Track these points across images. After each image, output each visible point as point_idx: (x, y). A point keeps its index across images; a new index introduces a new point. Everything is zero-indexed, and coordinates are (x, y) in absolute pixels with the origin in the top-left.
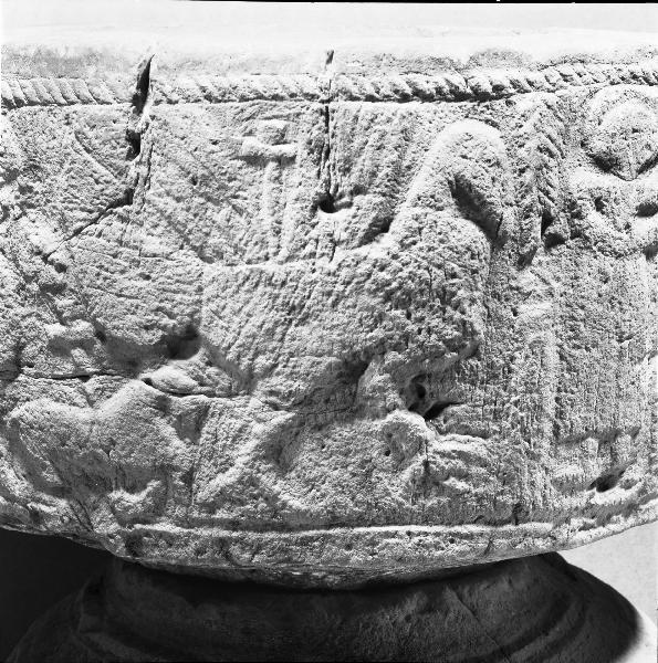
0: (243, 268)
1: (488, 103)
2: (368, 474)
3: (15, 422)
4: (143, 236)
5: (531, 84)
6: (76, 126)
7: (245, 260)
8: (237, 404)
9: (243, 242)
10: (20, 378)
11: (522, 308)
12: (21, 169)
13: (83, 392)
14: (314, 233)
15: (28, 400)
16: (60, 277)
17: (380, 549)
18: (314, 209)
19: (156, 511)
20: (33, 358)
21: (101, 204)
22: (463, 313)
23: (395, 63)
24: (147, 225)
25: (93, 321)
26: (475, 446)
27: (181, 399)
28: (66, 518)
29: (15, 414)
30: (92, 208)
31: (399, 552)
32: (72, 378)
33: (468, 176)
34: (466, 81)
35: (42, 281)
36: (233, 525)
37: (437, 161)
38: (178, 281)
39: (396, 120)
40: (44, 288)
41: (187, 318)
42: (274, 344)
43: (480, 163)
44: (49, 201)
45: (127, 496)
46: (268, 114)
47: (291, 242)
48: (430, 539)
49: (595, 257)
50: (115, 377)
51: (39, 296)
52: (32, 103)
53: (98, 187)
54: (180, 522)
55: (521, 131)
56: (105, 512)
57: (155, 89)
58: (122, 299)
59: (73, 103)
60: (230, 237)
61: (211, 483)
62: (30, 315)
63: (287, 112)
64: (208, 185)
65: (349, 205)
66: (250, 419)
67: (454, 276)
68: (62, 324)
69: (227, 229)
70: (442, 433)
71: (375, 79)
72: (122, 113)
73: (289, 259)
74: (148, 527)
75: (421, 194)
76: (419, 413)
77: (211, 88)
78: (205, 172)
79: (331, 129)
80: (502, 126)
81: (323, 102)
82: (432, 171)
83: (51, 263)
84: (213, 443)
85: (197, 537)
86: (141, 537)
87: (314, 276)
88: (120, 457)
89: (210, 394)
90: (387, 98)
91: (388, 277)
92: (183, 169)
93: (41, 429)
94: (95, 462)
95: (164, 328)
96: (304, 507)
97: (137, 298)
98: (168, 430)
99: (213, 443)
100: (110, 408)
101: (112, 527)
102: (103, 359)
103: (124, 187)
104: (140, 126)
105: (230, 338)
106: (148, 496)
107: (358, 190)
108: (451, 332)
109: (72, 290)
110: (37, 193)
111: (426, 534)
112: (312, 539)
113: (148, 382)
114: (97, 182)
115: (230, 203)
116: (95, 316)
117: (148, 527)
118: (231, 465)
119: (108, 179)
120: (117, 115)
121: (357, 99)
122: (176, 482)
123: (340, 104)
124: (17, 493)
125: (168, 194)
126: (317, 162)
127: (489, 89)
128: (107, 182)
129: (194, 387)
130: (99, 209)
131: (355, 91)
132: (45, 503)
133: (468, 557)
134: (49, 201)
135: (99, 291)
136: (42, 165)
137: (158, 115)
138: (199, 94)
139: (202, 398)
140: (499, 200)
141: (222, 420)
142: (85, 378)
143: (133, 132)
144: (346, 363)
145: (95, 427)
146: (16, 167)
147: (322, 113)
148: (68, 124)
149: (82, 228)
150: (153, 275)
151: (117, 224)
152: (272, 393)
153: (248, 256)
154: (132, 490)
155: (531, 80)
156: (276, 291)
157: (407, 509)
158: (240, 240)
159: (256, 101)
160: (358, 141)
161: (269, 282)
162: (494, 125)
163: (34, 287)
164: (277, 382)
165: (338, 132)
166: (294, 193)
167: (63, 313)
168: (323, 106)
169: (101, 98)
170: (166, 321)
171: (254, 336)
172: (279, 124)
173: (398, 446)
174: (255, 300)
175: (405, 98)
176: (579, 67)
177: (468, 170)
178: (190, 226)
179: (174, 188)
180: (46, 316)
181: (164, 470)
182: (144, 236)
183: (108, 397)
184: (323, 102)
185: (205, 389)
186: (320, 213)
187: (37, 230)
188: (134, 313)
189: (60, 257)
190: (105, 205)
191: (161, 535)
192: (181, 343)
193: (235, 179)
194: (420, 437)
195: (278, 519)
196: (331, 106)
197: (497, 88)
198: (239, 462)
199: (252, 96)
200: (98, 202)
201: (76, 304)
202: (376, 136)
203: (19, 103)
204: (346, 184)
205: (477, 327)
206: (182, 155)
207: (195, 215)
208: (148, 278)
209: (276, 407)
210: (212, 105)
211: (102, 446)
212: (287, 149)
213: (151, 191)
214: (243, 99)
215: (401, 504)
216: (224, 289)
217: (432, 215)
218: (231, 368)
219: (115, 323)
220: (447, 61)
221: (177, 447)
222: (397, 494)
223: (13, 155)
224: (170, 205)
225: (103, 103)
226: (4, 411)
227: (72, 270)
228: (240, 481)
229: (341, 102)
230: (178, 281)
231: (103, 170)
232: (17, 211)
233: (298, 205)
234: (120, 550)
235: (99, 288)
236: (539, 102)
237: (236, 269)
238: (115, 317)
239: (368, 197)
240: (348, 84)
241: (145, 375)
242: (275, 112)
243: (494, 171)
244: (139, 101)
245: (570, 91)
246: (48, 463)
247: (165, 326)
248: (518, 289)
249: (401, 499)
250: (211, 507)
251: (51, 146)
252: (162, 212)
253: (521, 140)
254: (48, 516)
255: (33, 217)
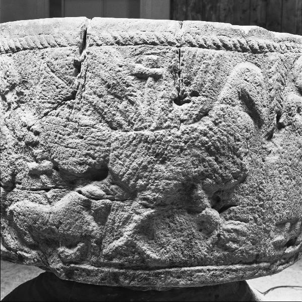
0: (132, 133)
1: (256, 55)
2: (190, 241)
3: (11, 212)
4: (81, 116)
5: (275, 48)
6: (47, 59)
7: (134, 128)
8: (126, 205)
9: (133, 119)
10: (14, 190)
11: (267, 158)
12: (18, 83)
13: (46, 197)
14: (170, 115)
15: (18, 200)
16: (36, 138)
17: (195, 278)
18: (171, 102)
19: (81, 258)
20: (21, 180)
21: (59, 99)
22: (242, 159)
23: (214, 29)
24: (82, 110)
25: (52, 160)
26: (242, 226)
27: (96, 202)
28: (36, 260)
29: (11, 208)
30: (53, 101)
31: (203, 279)
32: (40, 190)
33: (247, 90)
34: (247, 42)
35: (27, 140)
36: (121, 266)
37: (233, 81)
38: (98, 139)
39: (214, 59)
40: (28, 144)
41: (102, 159)
42: (147, 173)
43: (253, 84)
44: (31, 99)
45: (67, 250)
46: (149, 52)
47: (158, 119)
48: (218, 273)
49: (296, 136)
50: (63, 190)
51: (25, 148)
52: (25, 49)
53: (58, 90)
54: (93, 264)
55: (271, 70)
56: (56, 258)
57: (89, 38)
58: (68, 149)
59: (46, 47)
60: (126, 117)
61: (110, 245)
62: (19, 158)
63: (159, 51)
64: (117, 90)
65: (188, 102)
66: (132, 212)
67: (239, 140)
68: (37, 162)
69: (125, 112)
70: (227, 220)
71: (204, 37)
72: (72, 51)
73: (157, 128)
74: (77, 266)
75: (225, 97)
76: (216, 210)
77: (119, 38)
78: (115, 82)
79: (181, 61)
80: (262, 67)
81: (177, 47)
82: (231, 86)
83: (32, 131)
84: (113, 225)
85: (102, 272)
86: (73, 271)
87: (169, 138)
88: (64, 230)
89: (112, 200)
90: (209, 47)
91: (207, 140)
92: (103, 80)
93: (24, 215)
94: (51, 232)
95: (90, 164)
96: (157, 258)
97: (75, 148)
98: (89, 218)
99: (113, 225)
100: (60, 205)
101: (59, 265)
102: (57, 180)
103: (71, 90)
104: (81, 58)
105: (124, 169)
106: (78, 250)
107: (195, 94)
108: (235, 169)
109: (42, 145)
110: (25, 95)
111: (216, 270)
112: (161, 273)
113: (80, 192)
114: (57, 88)
115: (127, 99)
116: (53, 159)
117: (77, 266)
118: (122, 236)
119: (63, 86)
120: (69, 52)
121: (194, 46)
122: (92, 244)
123: (186, 48)
124: (12, 247)
125: (95, 93)
126: (174, 78)
127: (257, 47)
128: (62, 87)
129: (104, 195)
130: (58, 102)
131: (194, 42)
132: (25, 252)
133: (234, 280)
134: (31, 99)
135: (56, 145)
136: (29, 81)
137: (91, 52)
138: (113, 41)
139: (108, 201)
140: (260, 103)
141: (117, 213)
142: (47, 190)
143: (77, 61)
144: (183, 184)
145: (51, 215)
146: (15, 82)
147: (177, 53)
148: (43, 58)
149: (48, 112)
150: (85, 136)
151: (67, 110)
152: (144, 199)
153: (135, 126)
154: (70, 247)
155: (275, 46)
156: (149, 146)
157: (208, 258)
158: (132, 118)
159: (143, 45)
160: (195, 67)
161: (146, 141)
162: (259, 66)
163: (23, 143)
164: (148, 194)
165: (184, 63)
166: (161, 94)
167: (37, 156)
168: (177, 49)
169: (62, 44)
170: (91, 160)
171: (137, 169)
172: (155, 57)
173: (207, 227)
174: (138, 150)
175: (218, 48)
176: (293, 44)
177: (248, 87)
178: (106, 110)
179: (99, 89)
180: (28, 158)
181: (86, 237)
182: (81, 116)
183: (59, 200)
184: (177, 47)
185: (109, 196)
186: (174, 105)
187: (25, 115)
188: (74, 157)
189: (36, 128)
190: (61, 100)
191: (84, 270)
192: (98, 172)
193: (131, 86)
194: (217, 222)
195: (145, 263)
196: (182, 49)
197: (261, 47)
198: (126, 234)
199: (141, 42)
200: (57, 98)
201: (44, 152)
202: (204, 66)
203: (18, 49)
204: (188, 90)
205: (247, 167)
206: (102, 73)
207: (109, 105)
208: (82, 138)
209: (146, 207)
210: (120, 47)
211: (54, 225)
212: (158, 71)
213: (86, 92)
214: (136, 44)
215: (206, 255)
216: (121, 144)
217: (230, 108)
218: (123, 186)
219: (64, 161)
220: (239, 31)
221: (94, 226)
222: (204, 251)
223: (13, 76)
224: (95, 99)
225: (62, 46)
226: (6, 206)
227: (43, 135)
228: (126, 244)
229: (187, 47)
230: (98, 139)
231: (60, 81)
232: (15, 105)
233: (163, 100)
234: (63, 276)
235: (56, 143)
236: (278, 58)
237: (129, 133)
238: (64, 158)
239: (199, 97)
240: (191, 38)
241: (78, 189)
242: (153, 51)
243: (259, 89)
244: (83, 46)
245: (289, 54)
246: (27, 232)
247: (91, 162)
248: (265, 149)
249: (206, 253)
250: (109, 257)
251: (34, 70)
252: (91, 103)
253: (271, 75)
254: (27, 258)
255: (23, 108)
